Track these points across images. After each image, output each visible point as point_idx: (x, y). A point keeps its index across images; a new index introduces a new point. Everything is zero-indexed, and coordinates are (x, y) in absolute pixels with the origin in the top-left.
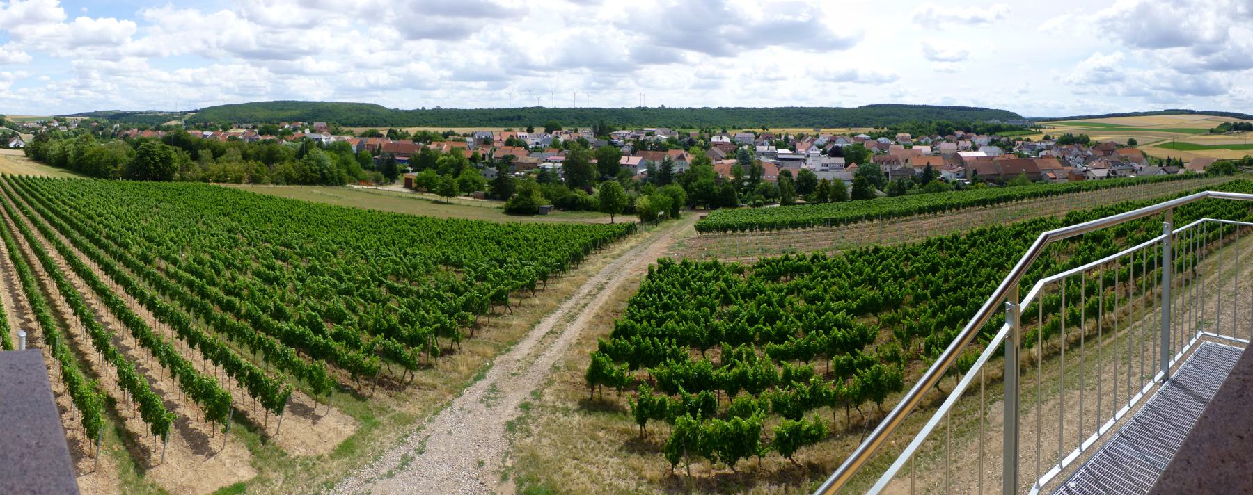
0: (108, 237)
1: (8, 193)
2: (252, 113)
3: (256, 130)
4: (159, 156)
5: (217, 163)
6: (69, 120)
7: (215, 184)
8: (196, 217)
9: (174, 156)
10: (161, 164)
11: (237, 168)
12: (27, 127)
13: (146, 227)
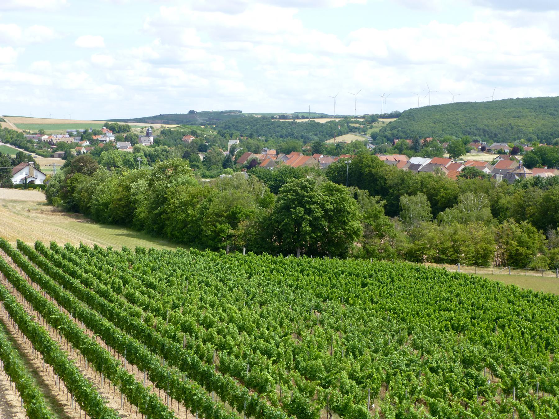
0: (224, 368)
1: (16, 283)
2: (513, 122)
3: (519, 157)
4: (322, 206)
5: (440, 222)
6: (136, 129)
7: (435, 265)
8: (397, 332)
9: (352, 206)
10: (325, 223)
11: (480, 234)
12: (50, 143)
13: (300, 349)
